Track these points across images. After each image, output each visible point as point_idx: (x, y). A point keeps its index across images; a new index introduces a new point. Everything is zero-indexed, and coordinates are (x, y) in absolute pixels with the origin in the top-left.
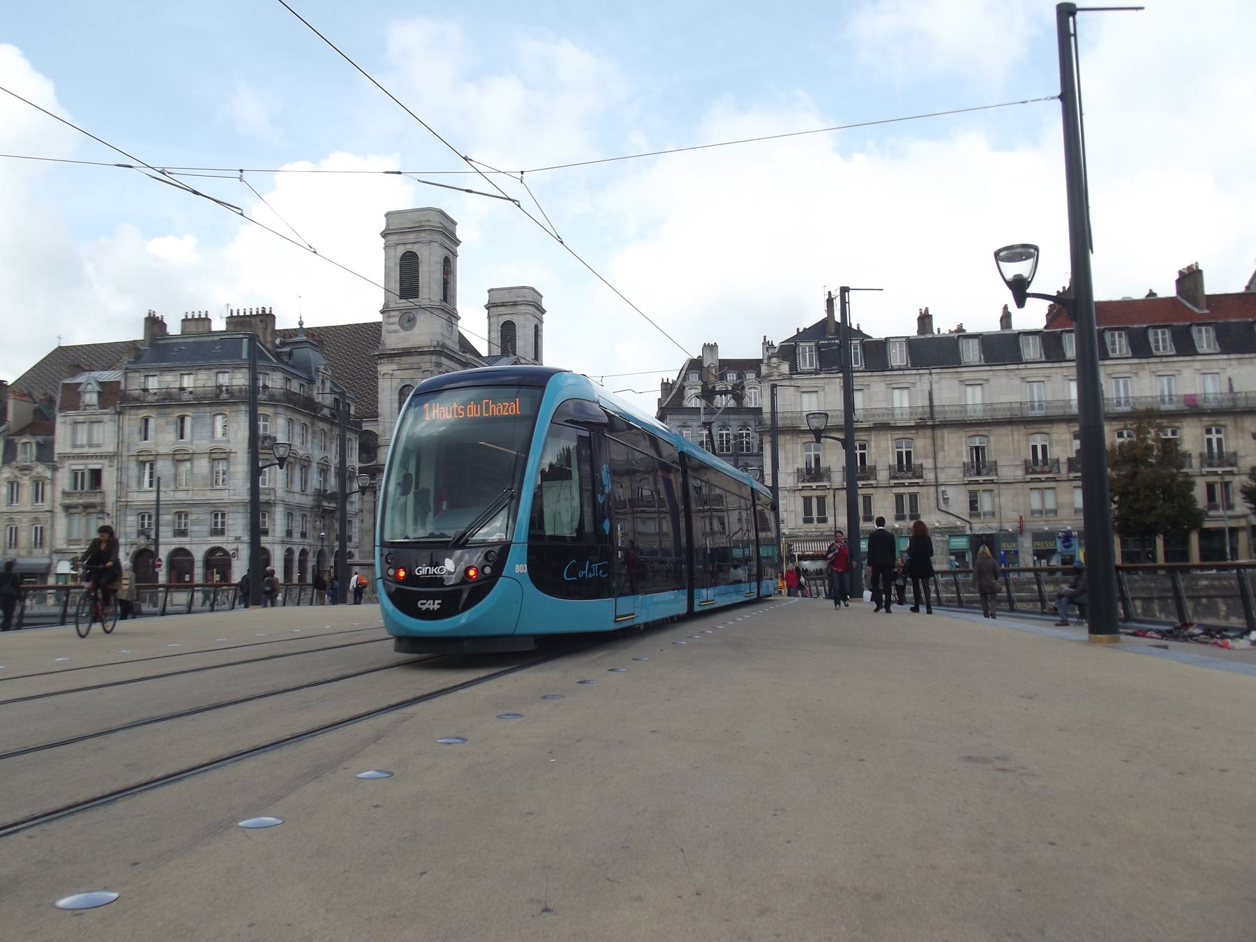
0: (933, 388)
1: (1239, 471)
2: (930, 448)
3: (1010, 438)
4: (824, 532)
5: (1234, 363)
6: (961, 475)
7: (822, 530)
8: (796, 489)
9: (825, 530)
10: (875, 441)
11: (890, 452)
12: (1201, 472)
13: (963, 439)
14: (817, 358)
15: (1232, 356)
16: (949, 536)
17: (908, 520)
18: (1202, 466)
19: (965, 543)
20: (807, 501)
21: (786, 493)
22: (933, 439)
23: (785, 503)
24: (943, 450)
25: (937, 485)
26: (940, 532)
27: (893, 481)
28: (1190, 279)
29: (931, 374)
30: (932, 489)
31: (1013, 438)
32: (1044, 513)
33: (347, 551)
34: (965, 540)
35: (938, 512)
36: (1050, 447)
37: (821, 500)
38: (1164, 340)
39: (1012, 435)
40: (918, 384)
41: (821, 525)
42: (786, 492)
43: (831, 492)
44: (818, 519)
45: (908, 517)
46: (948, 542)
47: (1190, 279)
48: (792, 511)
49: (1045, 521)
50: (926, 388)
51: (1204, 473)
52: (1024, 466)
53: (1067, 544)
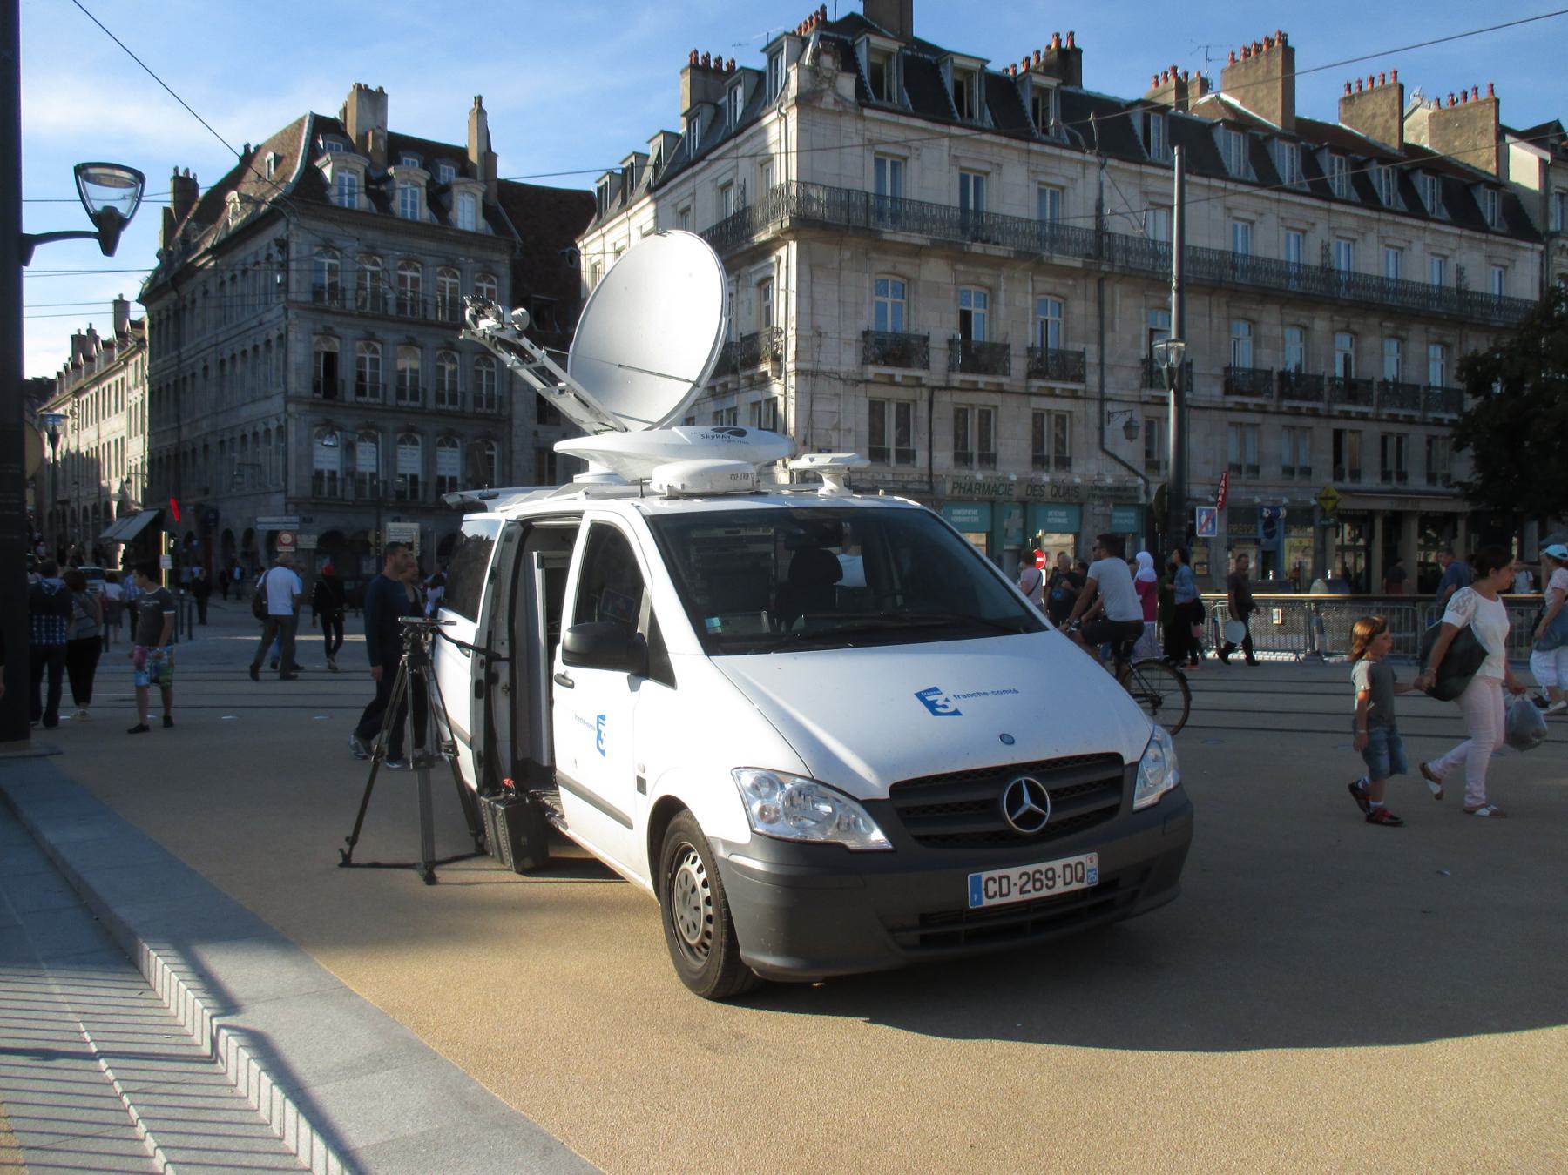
0: (1105, 198)
1: (1085, 392)
2: (1093, 322)
3: (1207, 319)
4: (908, 482)
5: (1465, 243)
6: (1137, 384)
7: (906, 479)
8: (858, 378)
9: (910, 479)
10: (1006, 291)
11: (1030, 321)
12: (1027, 387)
13: (1143, 311)
14: (902, 82)
15: (1466, 232)
16: (1115, 505)
17: (1052, 468)
18: (951, 368)
19: (1133, 521)
20: (876, 409)
21: (839, 387)
22: (1101, 304)
23: (834, 408)
24: (1113, 330)
25: (1102, 400)
26: (1102, 497)
27: (1037, 383)
28: (1066, 60)
29: (1102, 166)
30: (1093, 408)
31: (1211, 321)
32: (1244, 470)
33: (1452, 617)
34: (1132, 514)
35: (1100, 454)
36: (423, 281)
37: (904, 411)
38: (1388, 185)
39: (1210, 316)
40: (1080, 182)
41: (904, 468)
42: (838, 382)
43: (925, 393)
44: (898, 452)
45: (976, 458)
46: (1110, 517)
47: (1066, 60)
48: (849, 431)
49: (1245, 485)
50: (1092, 194)
51: (1336, 413)
52: (1223, 379)
53: (1269, 530)
